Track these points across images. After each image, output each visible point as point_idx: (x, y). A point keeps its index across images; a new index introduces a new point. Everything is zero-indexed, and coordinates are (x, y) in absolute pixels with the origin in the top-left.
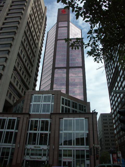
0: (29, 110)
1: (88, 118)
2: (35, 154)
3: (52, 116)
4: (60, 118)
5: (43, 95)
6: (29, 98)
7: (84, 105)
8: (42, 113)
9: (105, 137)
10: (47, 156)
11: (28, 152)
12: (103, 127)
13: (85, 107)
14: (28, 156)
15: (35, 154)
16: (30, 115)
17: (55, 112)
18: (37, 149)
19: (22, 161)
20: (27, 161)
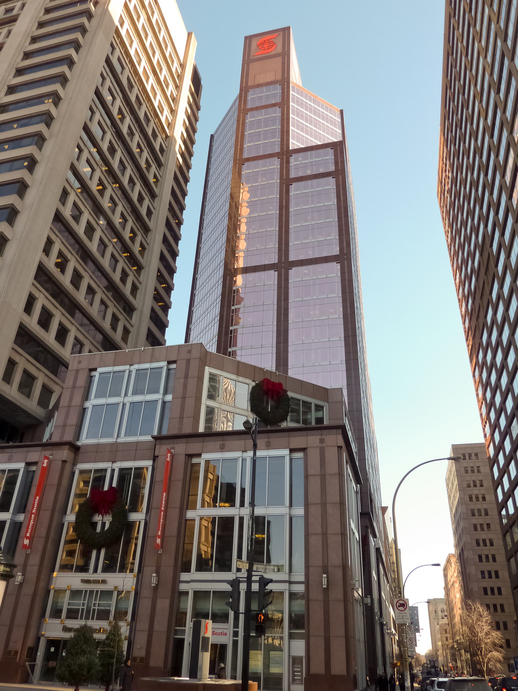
0: (78, 436)
1: (303, 450)
2: (83, 610)
3: (157, 447)
4: (190, 456)
5: (132, 368)
6: (82, 381)
7: (313, 401)
8: (123, 439)
9: (478, 544)
10: (111, 618)
11: (122, 606)
12: (467, 499)
13: (319, 408)
14: (58, 621)
15: (83, 610)
16: (76, 449)
17: (175, 432)
18: (91, 592)
19: (30, 643)
20: (51, 642)
